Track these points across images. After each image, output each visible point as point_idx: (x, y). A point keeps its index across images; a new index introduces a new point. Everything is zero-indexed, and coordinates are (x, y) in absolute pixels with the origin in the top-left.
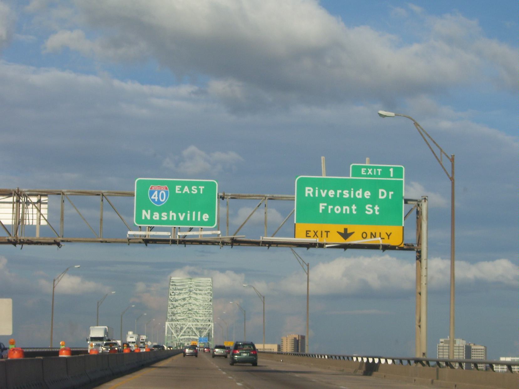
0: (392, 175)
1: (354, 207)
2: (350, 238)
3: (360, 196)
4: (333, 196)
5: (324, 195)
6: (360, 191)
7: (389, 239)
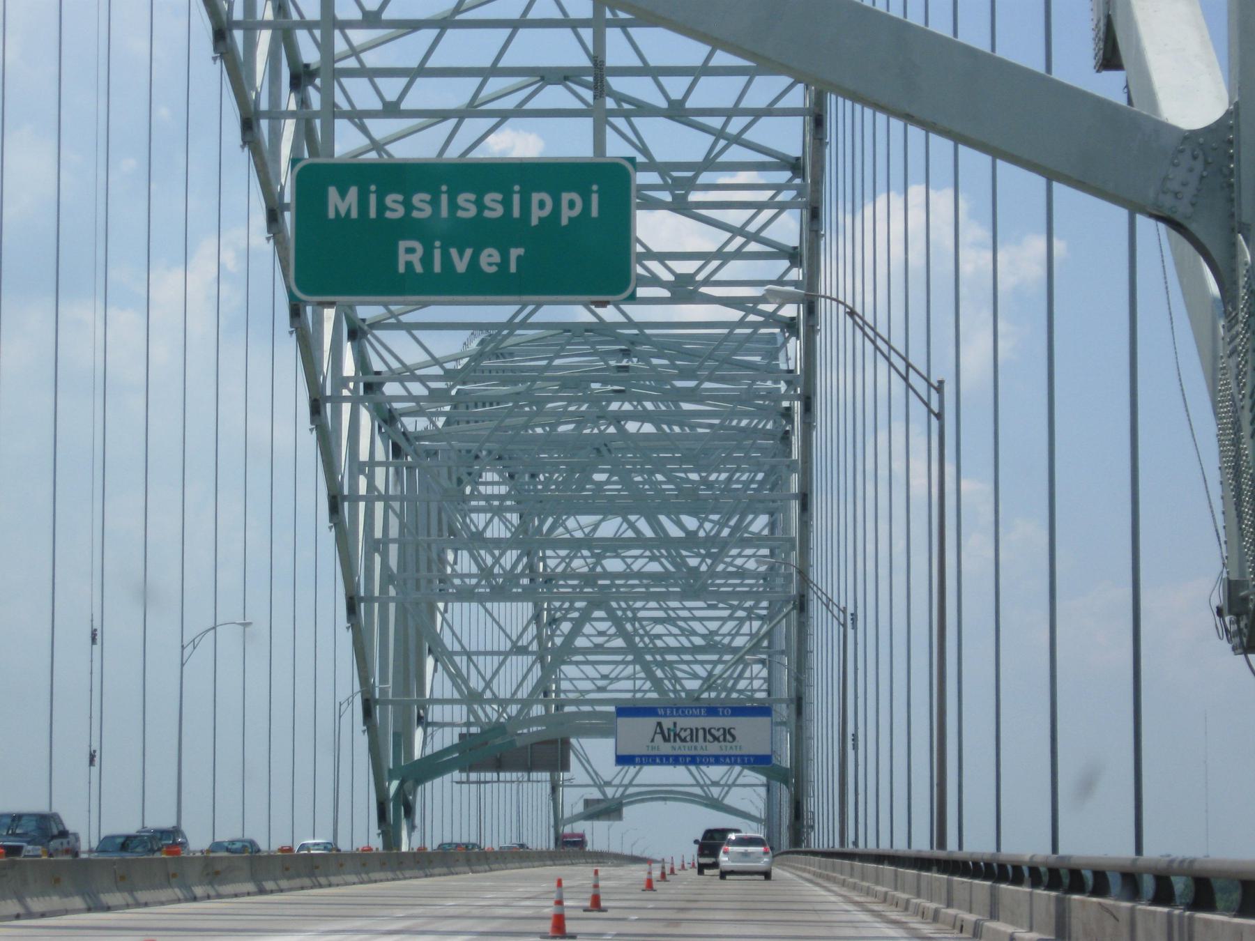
3: (566, 197)
4: (494, 269)
5: (461, 266)
6: (566, 215)
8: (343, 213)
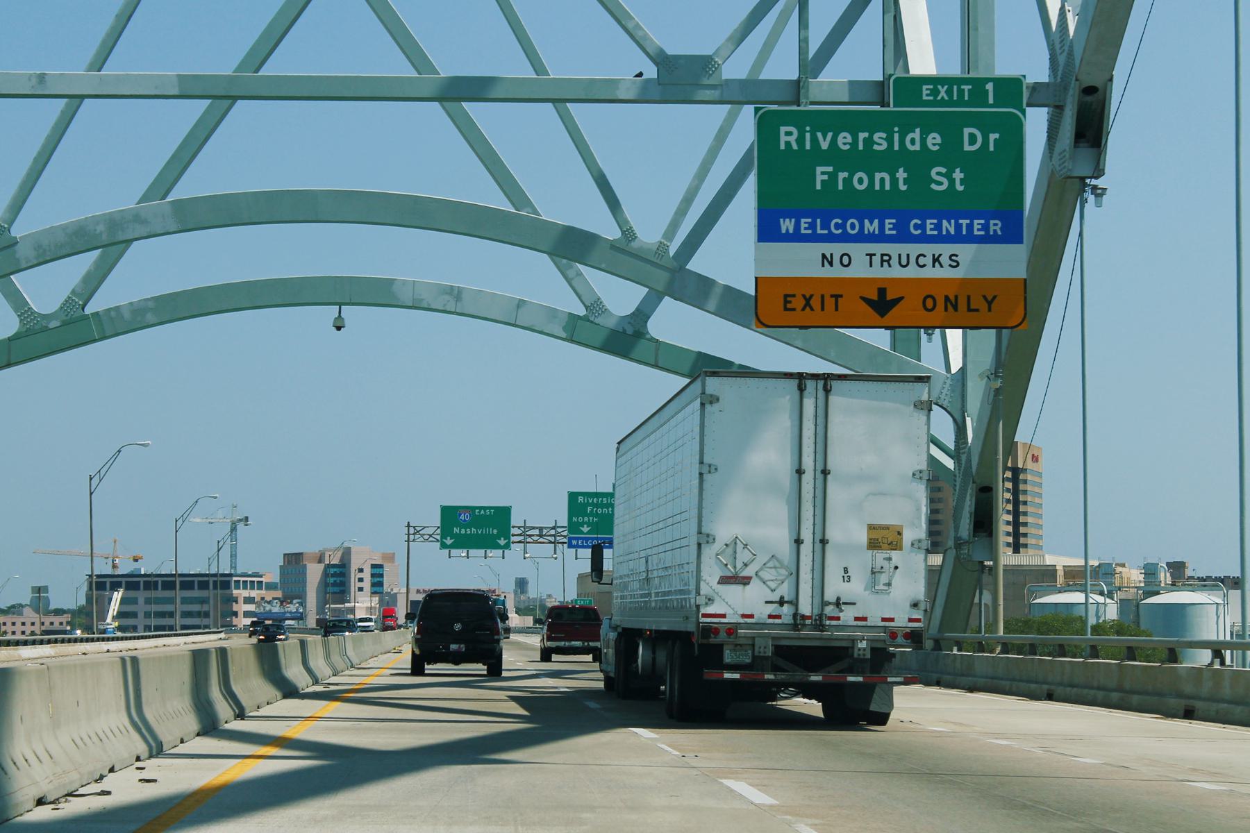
0: (991, 101)
1: (901, 174)
2: (895, 311)
3: (917, 147)
4: (847, 147)
5: (825, 146)
6: (917, 134)
7: (990, 310)
8: (871, 231)
